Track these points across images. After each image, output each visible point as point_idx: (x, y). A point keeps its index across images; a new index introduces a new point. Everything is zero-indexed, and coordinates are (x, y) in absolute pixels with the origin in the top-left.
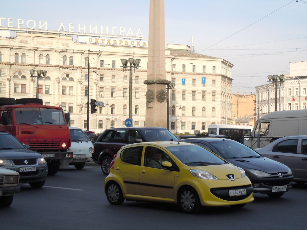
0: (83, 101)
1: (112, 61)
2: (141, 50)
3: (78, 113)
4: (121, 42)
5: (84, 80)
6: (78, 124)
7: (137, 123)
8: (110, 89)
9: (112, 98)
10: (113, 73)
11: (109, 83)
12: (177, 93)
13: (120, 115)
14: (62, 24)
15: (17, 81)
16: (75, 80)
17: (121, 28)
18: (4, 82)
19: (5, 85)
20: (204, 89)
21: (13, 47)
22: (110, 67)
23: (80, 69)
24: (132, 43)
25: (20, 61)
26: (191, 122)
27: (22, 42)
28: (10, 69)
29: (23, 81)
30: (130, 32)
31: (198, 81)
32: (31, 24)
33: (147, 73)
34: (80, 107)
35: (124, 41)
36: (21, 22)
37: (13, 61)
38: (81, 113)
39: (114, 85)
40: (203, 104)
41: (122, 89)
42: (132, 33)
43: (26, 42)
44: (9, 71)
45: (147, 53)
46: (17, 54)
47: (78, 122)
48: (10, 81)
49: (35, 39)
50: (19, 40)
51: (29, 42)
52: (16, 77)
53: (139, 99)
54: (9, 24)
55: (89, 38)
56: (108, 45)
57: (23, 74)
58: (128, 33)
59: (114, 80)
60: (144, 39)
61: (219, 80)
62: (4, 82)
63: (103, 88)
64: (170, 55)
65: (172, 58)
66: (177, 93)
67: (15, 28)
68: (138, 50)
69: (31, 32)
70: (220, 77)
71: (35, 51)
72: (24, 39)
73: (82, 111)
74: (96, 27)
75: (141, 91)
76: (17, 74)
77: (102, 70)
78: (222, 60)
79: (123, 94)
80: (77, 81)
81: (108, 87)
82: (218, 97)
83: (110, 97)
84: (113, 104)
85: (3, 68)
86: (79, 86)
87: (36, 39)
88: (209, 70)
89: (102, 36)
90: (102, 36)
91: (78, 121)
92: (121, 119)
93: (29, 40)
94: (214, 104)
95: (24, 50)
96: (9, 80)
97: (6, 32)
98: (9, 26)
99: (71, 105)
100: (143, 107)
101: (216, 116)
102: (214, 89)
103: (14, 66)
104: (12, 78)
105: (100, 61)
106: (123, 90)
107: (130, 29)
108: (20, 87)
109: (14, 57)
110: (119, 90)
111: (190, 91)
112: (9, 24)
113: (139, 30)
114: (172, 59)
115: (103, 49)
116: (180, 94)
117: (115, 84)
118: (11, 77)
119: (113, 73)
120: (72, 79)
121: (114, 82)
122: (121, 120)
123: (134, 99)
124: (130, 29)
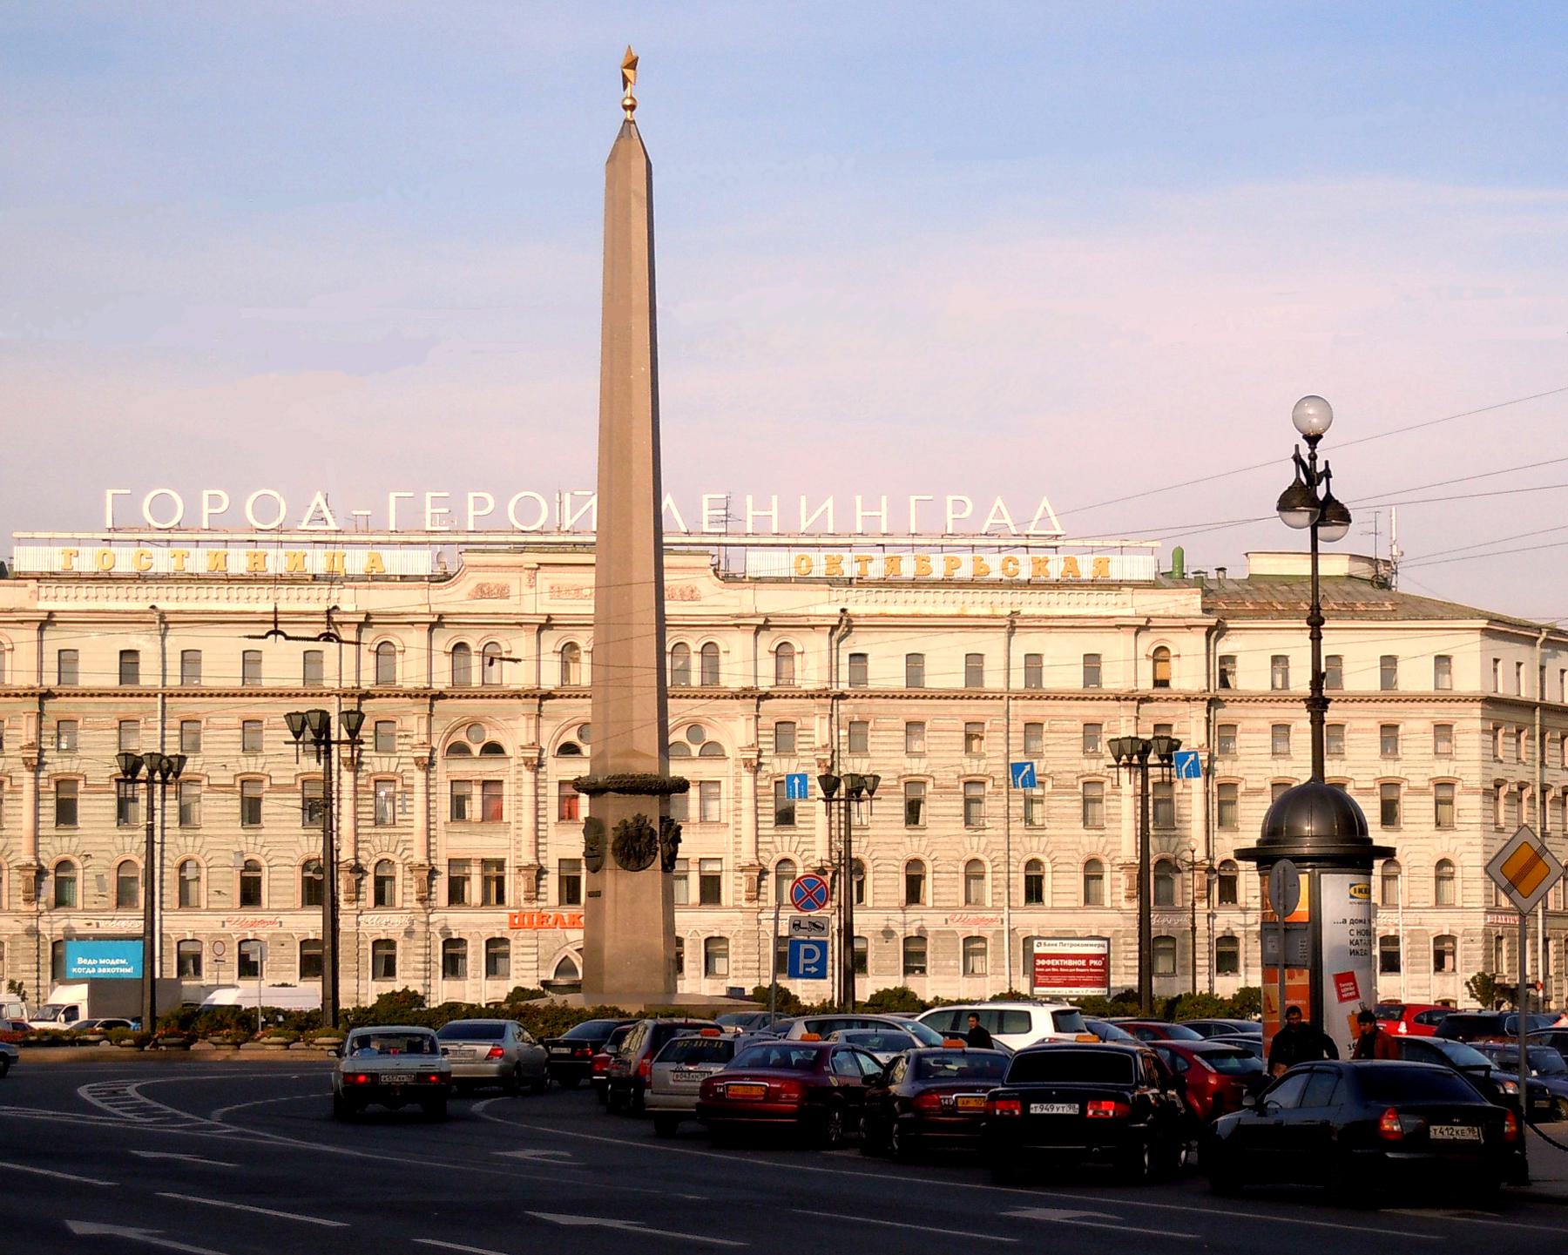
0: (366, 845)
1: (122, 653)
2: (1054, 596)
3: (745, 904)
4: (954, 564)
5: (772, 753)
6: (742, 957)
7: (980, 945)
8: (233, 786)
9: (908, 832)
10: (915, 709)
11: (894, 761)
12: (1243, 794)
13: (948, 908)
14: (1045, 503)
15: (461, 768)
16: (509, 752)
17: (950, 499)
18: (407, 774)
19: (408, 789)
20: (1390, 770)
21: (441, 616)
22: (899, 683)
23: (823, 701)
24: (1010, 565)
25: (476, 680)
26: (1434, 932)
27: (482, 592)
28: (758, 717)
29: (491, 768)
30: (999, 514)
31: (1357, 731)
32: (528, 509)
33: (589, 701)
34: (421, 880)
35: (966, 558)
36: (215, 501)
37: (442, 682)
38: (755, 904)
39: (917, 767)
40: (252, 845)
41: (1075, 787)
42: (1008, 520)
43: (503, 593)
44: (533, 730)
45: (592, 611)
46: (460, 647)
47: (746, 946)
48: (537, 773)
49: (539, 575)
50: (472, 585)
51: (514, 590)
52: (459, 750)
53: (1047, 832)
54: (428, 517)
55: (796, 552)
56: (888, 584)
57: (491, 736)
58: (990, 520)
59: (917, 746)
60: (1069, 543)
61: (1470, 723)
62: (407, 774)
63: (1451, 785)
64: (1200, 613)
65: (1210, 630)
66: (1243, 794)
67: (457, 532)
68: (1037, 596)
69: (523, 548)
70: (1476, 710)
71: (756, 633)
72: (493, 579)
73: (762, 897)
74: (829, 503)
75: (1053, 794)
76: (461, 736)
77: (858, 701)
78: (1483, 624)
79: (1433, 813)
80: (739, 755)
81: (1419, 781)
82: (1469, 806)
83: (230, 824)
84: (975, 860)
85: (406, 713)
86: (747, 780)
87: (546, 578)
88: (1415, 676)
89: (860, 540)
90: (860, 540)
91: (743, 942)
92: (952, 926)
93: (516, 582)
94: (1443, 845)
95: (491, 630)
96: (428, 765)
97: (782, 554)
98: (428, 528)
99: (710, 868)
100: (1066, 868)
101: (1458, 904)
102: (1442, 769)
103: (448, 701)
104: (438, 755)
105: (845, 660)
106: (1432, 789)
107: (999, 502)
108: (477, 791)
109: (772, 660)
110: (944, 790)
111: (1371, 785)
112: (428, 517)
113: (1045, 503)
114: (831, 634)
115: (861, 604)
116: (1260, 798)
117: (924, 762)
118: (541, 750)
119: (915, 710)
120: (493, 749)
121: (921, 755)
122: (954, 932)
123: (1020, 832)
124: (999, 502)
